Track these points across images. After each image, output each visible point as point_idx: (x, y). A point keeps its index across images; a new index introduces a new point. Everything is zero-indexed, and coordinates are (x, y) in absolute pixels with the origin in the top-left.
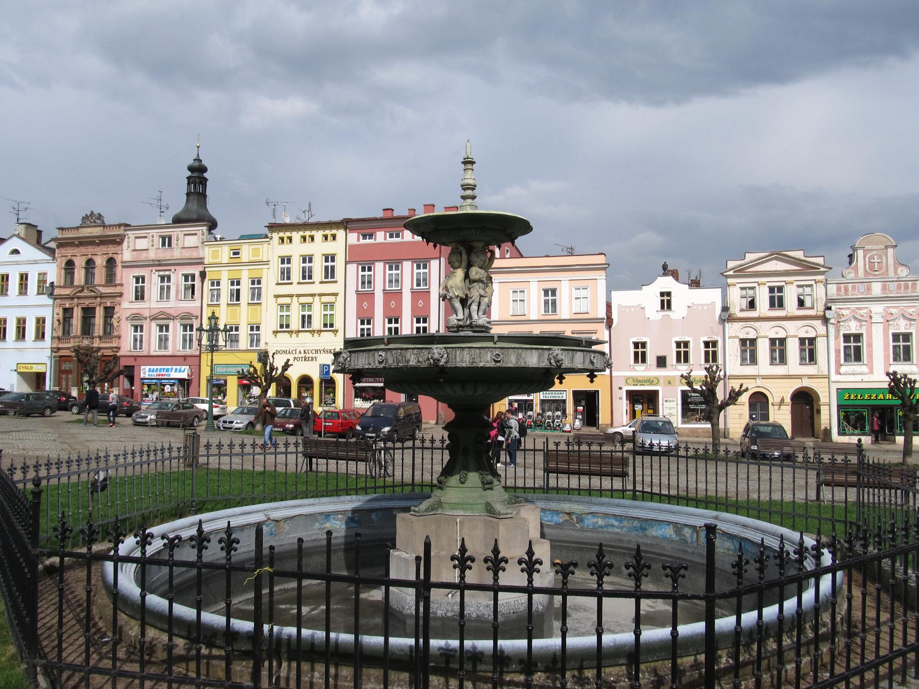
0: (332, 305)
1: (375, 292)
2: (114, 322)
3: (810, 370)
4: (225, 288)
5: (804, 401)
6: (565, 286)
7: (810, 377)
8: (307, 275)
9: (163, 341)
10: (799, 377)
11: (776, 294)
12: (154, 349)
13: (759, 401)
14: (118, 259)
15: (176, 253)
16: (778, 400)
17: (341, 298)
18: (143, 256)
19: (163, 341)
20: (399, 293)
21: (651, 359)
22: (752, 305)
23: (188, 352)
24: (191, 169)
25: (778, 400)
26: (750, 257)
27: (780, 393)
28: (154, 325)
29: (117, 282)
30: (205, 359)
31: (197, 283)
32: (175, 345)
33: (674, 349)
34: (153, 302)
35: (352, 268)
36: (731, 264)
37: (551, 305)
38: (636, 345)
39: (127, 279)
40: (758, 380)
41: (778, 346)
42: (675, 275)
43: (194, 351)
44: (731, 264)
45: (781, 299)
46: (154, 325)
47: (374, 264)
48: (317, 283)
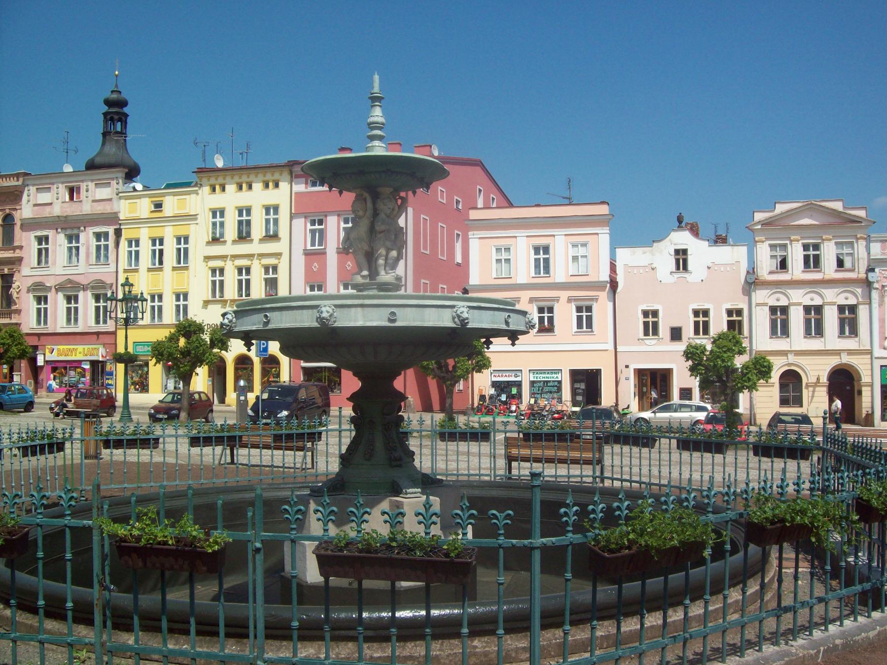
0: (275, 268)
1: (328, 250)
2: (13, 291)
3: (850, 344)
4: (145, 249)
5: (843, 382)
6: (561, 245)
7: (850, 352)
8: (244, 236)
9: (72, 315)
10: (837, 353)
11: (811, 252)
12: (59, 323)
13: (791, 382)
14: (17, 215)
15: (86, 207)
16: (814, 380)
17: (285, 258)
18: (47, 212)
19: (72, 315)
20: (323, 253)
21: (664, 331)
22: (783, 265)
23: (102, 328)
24: (108, 102)
25: (813, 380)
26: (781, 208)
27: (816, 371)
28: (60, 295)
29: (16, 244)
30: (121, 334)
31: (111, 243)
32: (87, 321)
33: (692, 319)
34: (59, 265)
35: (299, 223)
36: (759, 216)
37: (544, 266)
38: (646, 314)
39: (27, 241)
40: (790, 356)
41: (814, 313)
42: (695, 230)
43: (110, 326)
44: (759, 216)
45: (817, 259)
46: (60, 295)
47: (326, 216)
48: (229, 242)
